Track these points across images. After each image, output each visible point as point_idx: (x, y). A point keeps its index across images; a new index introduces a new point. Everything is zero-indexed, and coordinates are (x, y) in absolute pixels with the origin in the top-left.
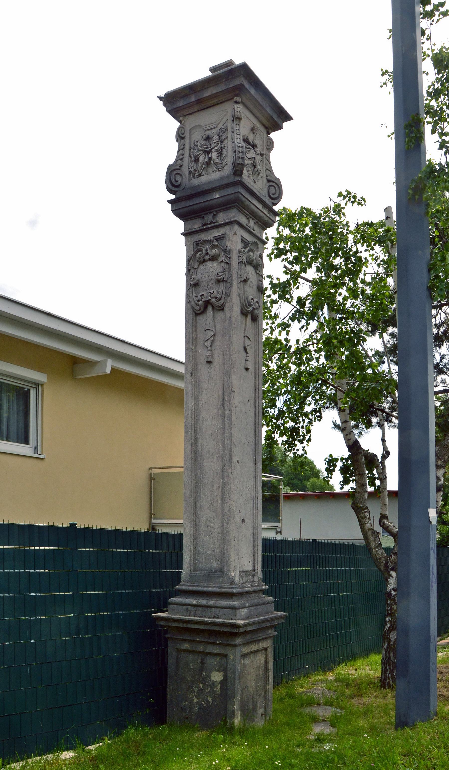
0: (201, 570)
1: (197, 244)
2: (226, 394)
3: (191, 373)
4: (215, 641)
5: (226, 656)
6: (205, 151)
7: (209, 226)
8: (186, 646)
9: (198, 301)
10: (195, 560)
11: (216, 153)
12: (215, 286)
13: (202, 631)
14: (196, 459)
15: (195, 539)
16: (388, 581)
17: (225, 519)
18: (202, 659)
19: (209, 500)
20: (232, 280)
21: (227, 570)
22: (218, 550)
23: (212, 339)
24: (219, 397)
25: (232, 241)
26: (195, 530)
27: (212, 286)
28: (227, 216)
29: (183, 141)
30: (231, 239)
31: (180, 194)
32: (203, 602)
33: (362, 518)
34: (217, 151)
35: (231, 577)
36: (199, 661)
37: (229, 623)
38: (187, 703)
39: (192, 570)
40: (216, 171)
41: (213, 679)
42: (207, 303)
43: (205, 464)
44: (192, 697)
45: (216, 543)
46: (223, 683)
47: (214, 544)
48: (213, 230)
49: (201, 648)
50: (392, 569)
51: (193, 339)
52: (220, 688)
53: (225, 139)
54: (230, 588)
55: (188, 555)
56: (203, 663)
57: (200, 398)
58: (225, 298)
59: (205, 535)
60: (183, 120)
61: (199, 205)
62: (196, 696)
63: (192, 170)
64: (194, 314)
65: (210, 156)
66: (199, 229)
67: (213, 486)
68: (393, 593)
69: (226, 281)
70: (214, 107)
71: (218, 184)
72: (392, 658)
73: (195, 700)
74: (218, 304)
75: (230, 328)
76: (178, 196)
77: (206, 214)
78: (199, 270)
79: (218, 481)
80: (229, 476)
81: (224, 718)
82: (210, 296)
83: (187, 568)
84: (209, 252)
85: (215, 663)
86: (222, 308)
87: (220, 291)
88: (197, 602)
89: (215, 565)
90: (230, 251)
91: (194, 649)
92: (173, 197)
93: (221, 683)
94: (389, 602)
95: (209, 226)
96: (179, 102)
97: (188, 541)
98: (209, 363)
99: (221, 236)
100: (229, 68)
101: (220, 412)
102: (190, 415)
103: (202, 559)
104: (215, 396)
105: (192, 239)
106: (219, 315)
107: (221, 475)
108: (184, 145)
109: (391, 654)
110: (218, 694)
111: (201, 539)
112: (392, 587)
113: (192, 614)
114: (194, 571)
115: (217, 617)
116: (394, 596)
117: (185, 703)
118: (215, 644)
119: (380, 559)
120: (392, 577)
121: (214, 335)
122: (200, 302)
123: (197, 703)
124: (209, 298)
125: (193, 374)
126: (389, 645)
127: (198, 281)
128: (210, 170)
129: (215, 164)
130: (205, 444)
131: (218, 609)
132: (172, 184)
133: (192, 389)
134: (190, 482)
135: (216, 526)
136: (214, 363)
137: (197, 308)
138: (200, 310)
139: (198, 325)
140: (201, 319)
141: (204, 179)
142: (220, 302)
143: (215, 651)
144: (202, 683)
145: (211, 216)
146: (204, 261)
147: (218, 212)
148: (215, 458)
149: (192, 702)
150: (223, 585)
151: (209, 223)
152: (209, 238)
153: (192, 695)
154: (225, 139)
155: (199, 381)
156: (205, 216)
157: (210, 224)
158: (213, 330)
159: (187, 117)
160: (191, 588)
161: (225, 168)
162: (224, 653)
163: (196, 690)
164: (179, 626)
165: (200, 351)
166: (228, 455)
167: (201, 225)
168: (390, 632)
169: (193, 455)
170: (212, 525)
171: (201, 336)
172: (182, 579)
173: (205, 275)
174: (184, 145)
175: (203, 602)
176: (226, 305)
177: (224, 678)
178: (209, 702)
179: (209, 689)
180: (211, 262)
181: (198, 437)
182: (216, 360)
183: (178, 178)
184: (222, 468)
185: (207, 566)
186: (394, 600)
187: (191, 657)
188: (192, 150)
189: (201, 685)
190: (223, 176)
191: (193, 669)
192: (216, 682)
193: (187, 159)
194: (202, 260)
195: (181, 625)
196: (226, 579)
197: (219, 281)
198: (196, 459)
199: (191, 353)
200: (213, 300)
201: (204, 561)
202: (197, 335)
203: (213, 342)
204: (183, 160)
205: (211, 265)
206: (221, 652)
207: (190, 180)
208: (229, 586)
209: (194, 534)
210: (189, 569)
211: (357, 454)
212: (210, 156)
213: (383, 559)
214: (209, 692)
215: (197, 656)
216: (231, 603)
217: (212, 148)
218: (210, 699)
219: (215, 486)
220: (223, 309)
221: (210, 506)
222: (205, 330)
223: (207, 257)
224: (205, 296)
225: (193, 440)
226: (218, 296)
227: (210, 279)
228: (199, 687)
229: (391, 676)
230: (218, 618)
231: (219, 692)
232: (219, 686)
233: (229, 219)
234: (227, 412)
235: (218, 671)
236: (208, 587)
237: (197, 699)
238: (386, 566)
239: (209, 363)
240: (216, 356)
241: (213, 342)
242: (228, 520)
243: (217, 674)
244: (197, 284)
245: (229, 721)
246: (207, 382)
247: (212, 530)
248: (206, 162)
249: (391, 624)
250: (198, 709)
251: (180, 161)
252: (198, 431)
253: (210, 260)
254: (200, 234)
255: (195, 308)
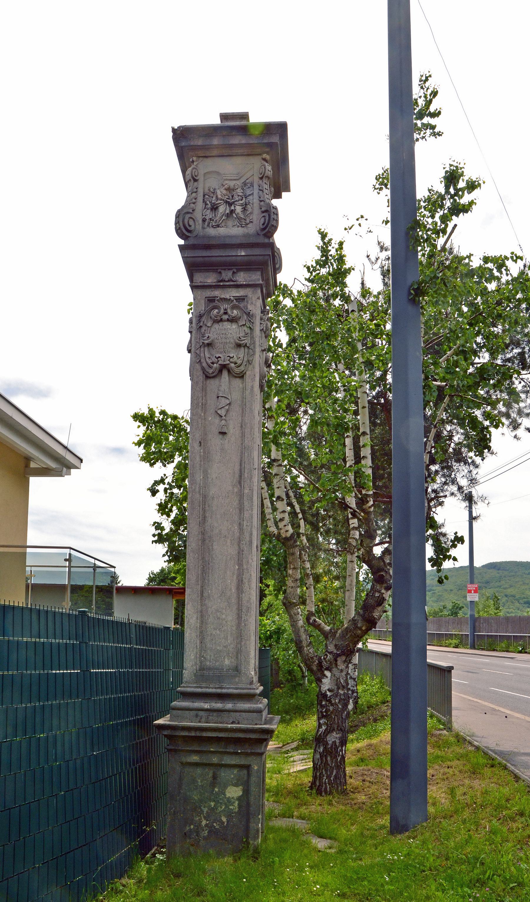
0: (209, 669)
1: (211, 300)
2: (246, 471)
3: (200, 442)
4: (236, 751)
5: (248, 767)
6: (226, 202)
7: (228, 283)
8: (195, 758)
9: (213, 363)
10: (201, 657)
11: (241, 207)
12: (233, 351)
13: (219, 740)
14: (204, 540)
15: (201, 632)
16: (321, 681)
17: (243, 610)
18: (214, 773)
19: (220, 588)
20: (254, 347)
21: (245, 668)
22: (232, 646)
23: (227, 407)
24: (234, 473)
25: (255, 305)
26: (202, 622)
27: (230, 349)
28: (250, 277)
29: (196, 183)
30: (254, 302)
31: (191, 241)
32: (219, 705)
33: (295, 615)
34: (242, 205)
35: (250, 676)
36: (211, 775)
37: (260, 728)
38: (192, 827)
39: (198, 669)
40: (238, 227)
41: (228, 795)
42: (224, 367)
43: (215, 547)
44: (199, 819)
45: (229, 638)
46: (245, 800)
47: (226, 638)
48: (231, 289)
49: (215, 760)
50: (327, 669)
51: (202, 404)
52: (238, 805)
53: (250, 195)
54: (250, 689)
55: (193, 651)
56: (215, 777)
57: (209, 471)
58: (246, 365)
59: (214, 629)
60: (196, 161)
61: (218, 259)
62: (205, 817)
63: (207, 218)
64: (204, 377)
65: (233, 208)
66: (214, 284)
67: (226, 572)
68: (329, 694)
69: (248, 347)
70: (228, 159)
71: (238, 241)
72: (329, 762)
73: (204, 823)
74: (237, 370)
75: (252, 399)
76: (187, 243)
77: (225, 269)
78: (213, 329)
79: (232, 568)
80: (248, 562)
81: (244, 840)
82: (229, 360)
83: (192, 666)
84: (229, 311)
85: (232, 776)
86: (241, 376)
87: (242, 356)
88: (210, 706)
89: (227, 662)
90: (252, 316)
91: (205, 761)
92: (182, 242)
93: (239, 799)
94: (324, 703)
95: (228, 283)
96: (189, 143)
97: (194, 635)
98: (223, 433)
99: (241, 298)
100: (243, 123)
101: (236, 490)
102: (197, 490)
103: (210, 656)
104: (230, 472)
105: (204, 293)
106: (237, 382)
107: (237, 559)
108: (197, 189)
109: (329, 758)
110: (235, 812)
111: (209, 633)
112: (327, 688)
113: (203, 720)
114: (200, 670)
115: (237, 722)
116: (330, 697)
117: (190, 826)
118: (237, 753)
119: (312, 658)
120: (327, 677)
121: (230, 404)
122: (215, 365)
123: (206, 825)
124: (228, 362)
125: (202, 444)
126: (325, 748)
127: (212, 341)
128: (230, 223)
129: (239, 219)
130: (216, 525)
131: (238, 714)
132: (182, 229)
133: (201, 461)
134: (197, 567)
135: (230, 618)
136: (229, 435)
137: (211, 371)
138: (213, 373)
139: (208, 389)
140: (213, 384)
141: (222, 231)
142: (239, 368)
143: (233, 762)
144: (214, 801)
145: (230, 273)
146: (221, 320)
147: (239, 270)
148: (229, 541)
149: (200, 825)
150: (240, 686)
151: (227, 280)
152: (228, 297)
153: (200, 816)
154: (250, 195)
155: (209, 453)
156: (223, 272)
157: (228, 281)
158: (229, 398)
159: (201, 159)
160: (199, 690)
161: (248, 226)
162: (246, 763)
163: (205, 810)
164: (190, 735)
165: (210, 418)
166: (248, 539)
167: (215, 281)
168: (327, 735)
169: (200, 536)
170: (224, 616)
171: (211, 402)
172: (184, 680)
173: (221, 336)
174: (197, 189)
175: (219, 705)
176: (247, 373)
177: (243, 792)
178: (224, 823)
179: (223, 807)
180: (230, 323)
181: (207, 515)
182: (231, 431)
183: (191, 222)
184: (239, 553)
185: (217, 664)
186: (330, 701)
187: (199, 771)
188: (207, 196)
189: (212, 804)
190: (248, 233)
191: (202, 786)
192: (233, 798)
193: (200, 205)
194: (219, 318)
195: (193, 734)
196: (243, 679)
197: (239, 346)
198: (204, 540)
199: (200, 420)
200: (233, 365)
201: (212, 657)
202: (206, 401)
203: (228, 411)
204: (196, 204)
205: (229, 327)
206: (242, 763)
207: (203, 228)
208: (249, 686)
209: (201, 627)
210: (195, 667)
211: (294, 547)
212: (233, 208)
213: (315, 658)
214: (224, 810)
215: (207, 770)
216: (255, 706)
217: (236, 201)
218: (224, 819)
219: (228, 573)
220: (242, 377)
221: (221, 595)
222: (218, 397)
223: (225, 317)
224: (222, 359)
225: (201, 519)
226: (239, 362)
227: (228, 341)
228: (210, 806)
229: (328, 781)
230: (238, 723)
231: (237, 810)
232: (237, 802)
233: (251, 281)
234: (246, 491)
235: (236, 785)
236: (221, 688)
237: (207, 820)
238: (320, 665)
239: (223, 433)
240: (231, 427)
241: (228, 411)
242: (247, 612)
243: (235, 788)
244: (211, 344)
245: (251, 842)
246: (219, 454)
247: (224, 622)
248: (228, 213)
249: (328, 726)
250: (208, 832)
251: (192, 205)
252: (207, 508)
253: (228, 320)
254: (213, 289)
255: (207, 370)
